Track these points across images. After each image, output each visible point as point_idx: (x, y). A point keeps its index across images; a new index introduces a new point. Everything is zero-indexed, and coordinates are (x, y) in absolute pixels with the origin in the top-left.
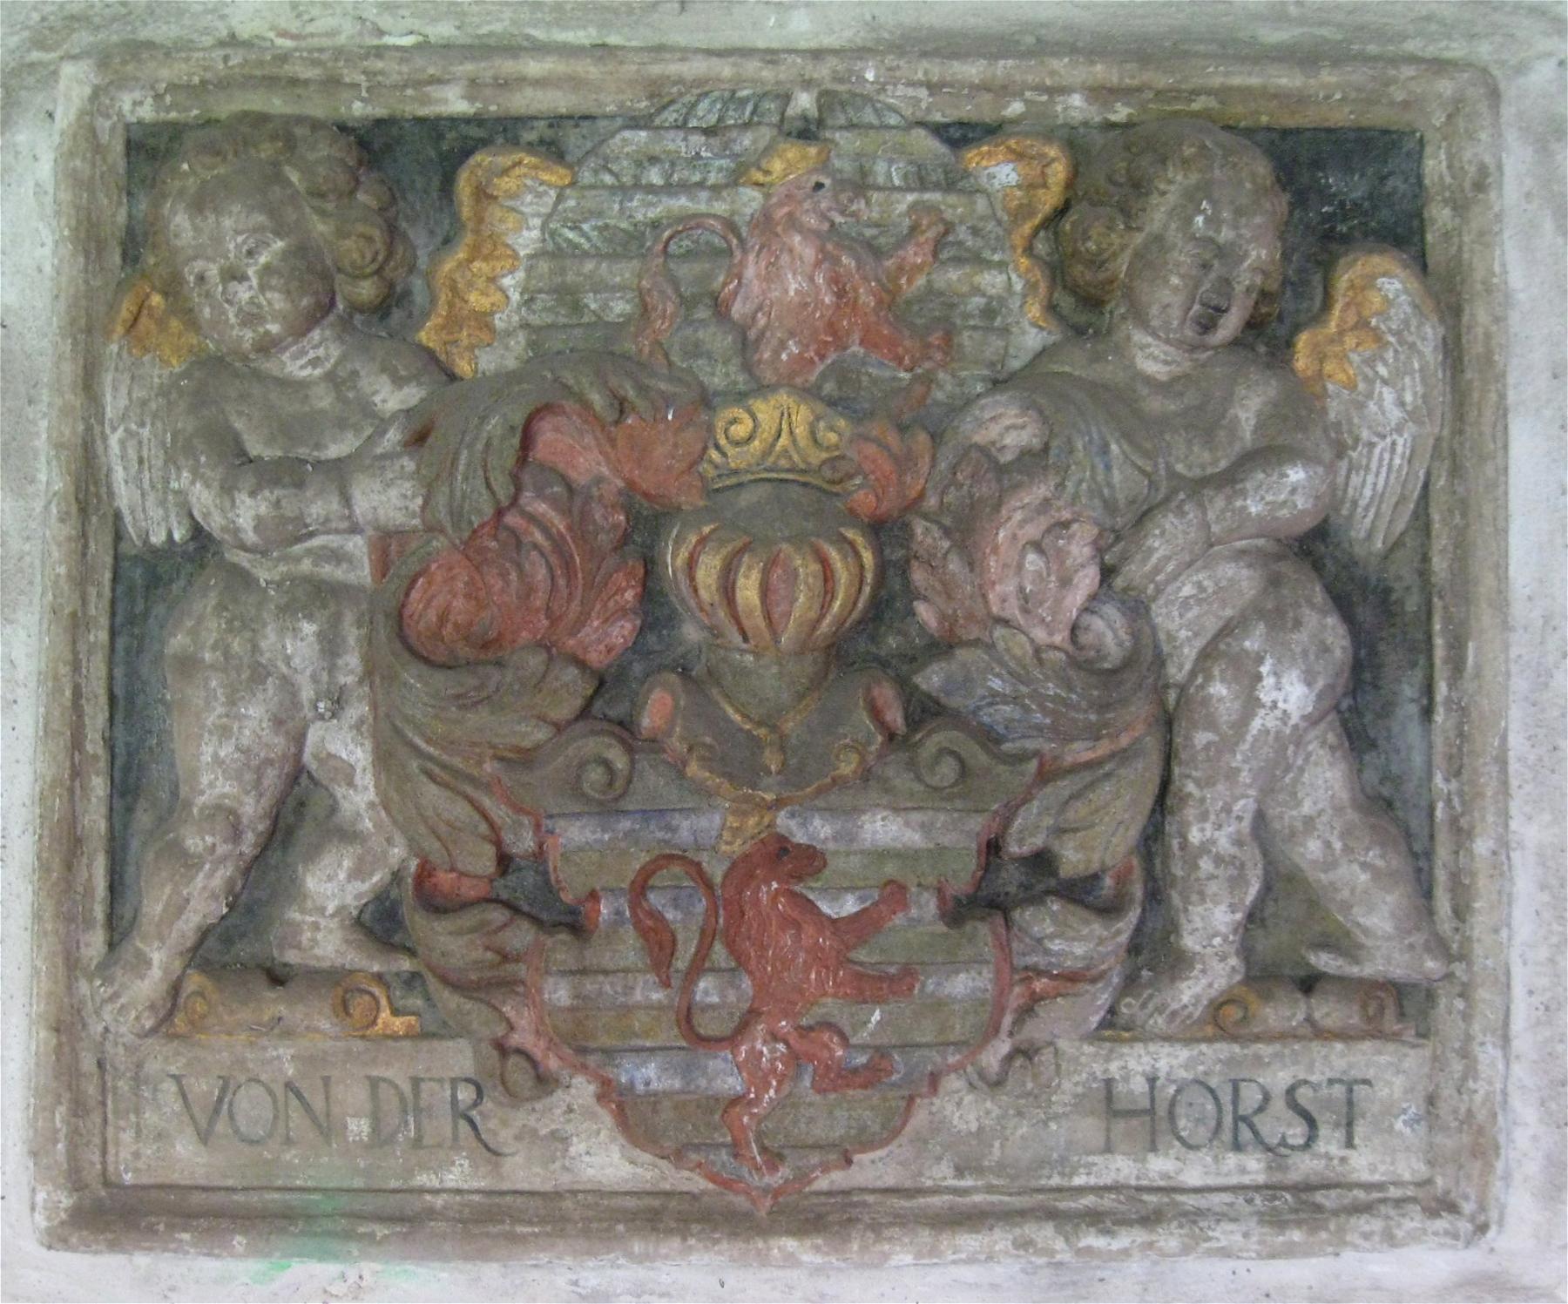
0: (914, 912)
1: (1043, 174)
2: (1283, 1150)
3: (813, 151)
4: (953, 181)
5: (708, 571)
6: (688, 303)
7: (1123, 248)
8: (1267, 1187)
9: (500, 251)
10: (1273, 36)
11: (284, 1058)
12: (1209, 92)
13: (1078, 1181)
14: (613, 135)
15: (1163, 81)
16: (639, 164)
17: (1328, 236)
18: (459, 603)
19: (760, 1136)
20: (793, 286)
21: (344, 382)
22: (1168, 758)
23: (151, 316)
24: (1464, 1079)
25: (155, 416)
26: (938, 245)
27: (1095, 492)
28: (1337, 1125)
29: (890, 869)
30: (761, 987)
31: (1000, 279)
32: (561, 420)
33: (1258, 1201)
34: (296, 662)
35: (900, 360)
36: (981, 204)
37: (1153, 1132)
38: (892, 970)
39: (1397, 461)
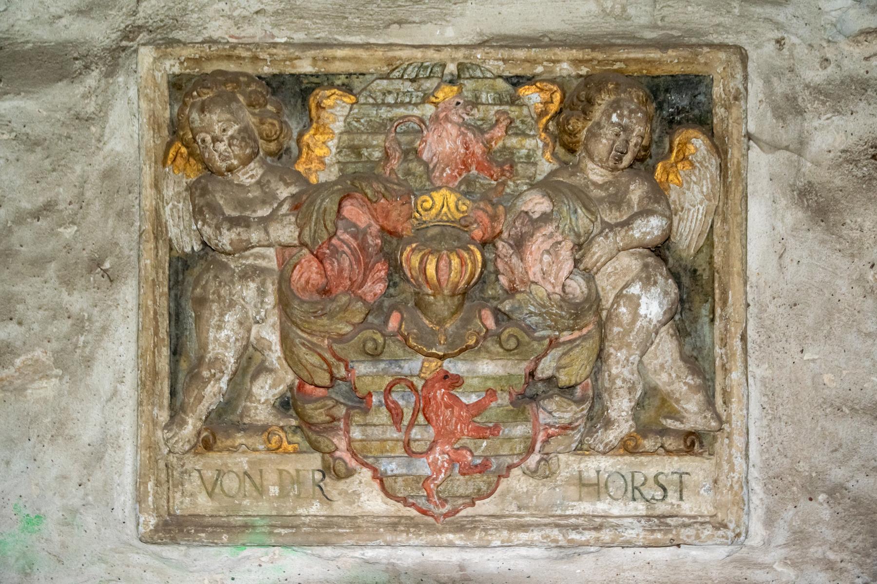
0: (499, 401)
1: (551, 97)
2: (653, 501)
3: (455, 88)
4: (514, 101)
5: (415, 261)
6: (406, 153)
7: (583, 128)
8: (647, 516)
9: (327, 130)
10: (649, 35)
11: (242, 461)
12: (620, 61)
13: (568, 513)
14: (373, 82)
15: (601, 56)
16: (384, 94)
17: (671, 122)
18: (314, 276)
19: (437, 492)
20: (448, 146)
21: (264, 185)
22: (603, 339)
23: (182, 156)
24: (729, 472)
25: (185, 199)
26: (508, 128)
27: (571, 229)
28: (676, 491)
29: (490, 384)
30: (438, 433)
31: (533, 142)
32: (354, 201)
33: (643, 522)
34: (247, 299)
35: (492, 176)
36: (525, 111)
37: (599, 493)
38: (491, 425)
39: (700, 216)
